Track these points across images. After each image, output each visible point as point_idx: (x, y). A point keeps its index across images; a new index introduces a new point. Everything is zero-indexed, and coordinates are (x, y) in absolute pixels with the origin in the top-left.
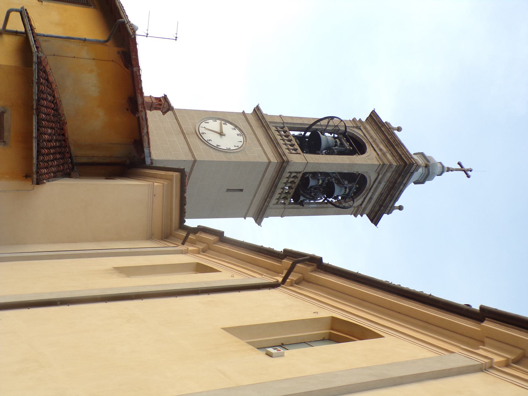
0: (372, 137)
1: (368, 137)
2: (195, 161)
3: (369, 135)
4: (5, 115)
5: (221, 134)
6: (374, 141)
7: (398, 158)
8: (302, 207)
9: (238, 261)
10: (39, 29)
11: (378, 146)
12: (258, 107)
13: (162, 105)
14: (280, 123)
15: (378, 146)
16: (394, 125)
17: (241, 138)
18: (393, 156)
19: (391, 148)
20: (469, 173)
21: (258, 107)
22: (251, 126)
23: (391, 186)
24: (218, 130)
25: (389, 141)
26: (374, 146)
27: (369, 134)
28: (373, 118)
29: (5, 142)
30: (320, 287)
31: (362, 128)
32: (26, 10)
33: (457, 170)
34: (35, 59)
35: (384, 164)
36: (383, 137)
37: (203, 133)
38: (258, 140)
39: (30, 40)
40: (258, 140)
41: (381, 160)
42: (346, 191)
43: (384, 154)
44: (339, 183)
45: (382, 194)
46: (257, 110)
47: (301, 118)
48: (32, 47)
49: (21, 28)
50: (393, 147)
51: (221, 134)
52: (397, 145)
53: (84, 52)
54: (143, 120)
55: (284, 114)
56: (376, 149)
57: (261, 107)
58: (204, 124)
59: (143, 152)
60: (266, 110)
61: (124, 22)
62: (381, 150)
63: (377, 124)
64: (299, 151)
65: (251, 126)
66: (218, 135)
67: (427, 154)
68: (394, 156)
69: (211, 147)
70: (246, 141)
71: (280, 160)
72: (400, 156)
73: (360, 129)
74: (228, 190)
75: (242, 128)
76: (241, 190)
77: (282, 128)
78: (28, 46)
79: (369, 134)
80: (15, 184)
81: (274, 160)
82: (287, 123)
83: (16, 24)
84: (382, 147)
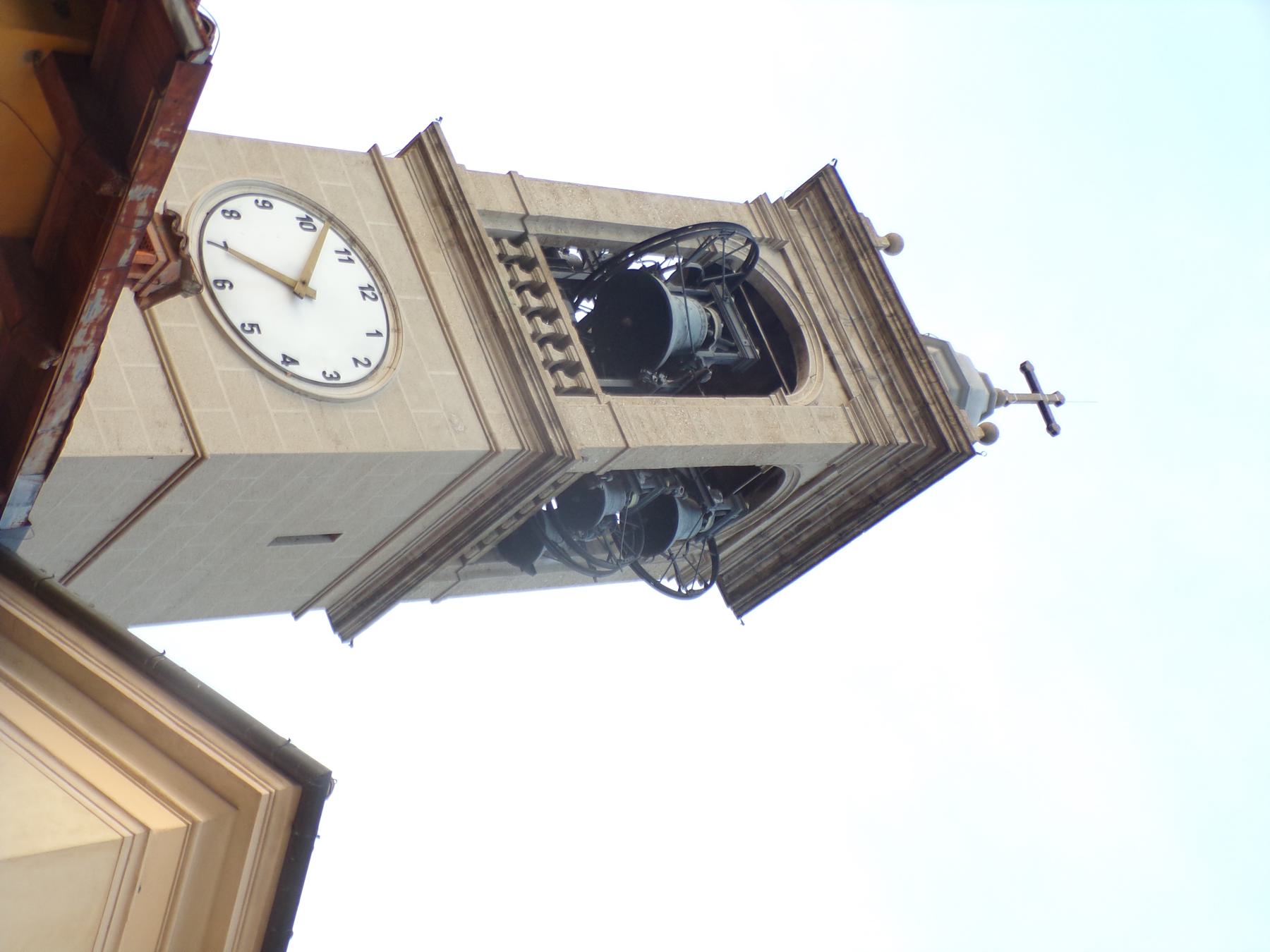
0: (823, 299)
1: (812, 298)
2: (196, 460)
3: (798, 274)
5: (298, 288)
6: (832, 321)
7: (913, 411)
8: (526, 576)
11: (845, 347)
12: (433, 129)
13: (152, 271)
14: (511, 216)
15: (845, 347)
17: (375, 314)
18: (896, 399)
20: (1052, 408)
21: (433, 129)
22: (410, 242)
23: (852, 504)
25: (884, 327)
26: (834, 347)
27: (814, 281)
28: (823, 195)
31: (788, 249)
33: (1022, 399)
35: (870, 444)
36: (862, 306)
37: (223, 283)
41: (863, 424)
42: (704, 525)
43: (867, 390)
44: (700, 506)
45: (808, 522)
46: (427, 149)
47: (585, 190)
51: (298, 288)
52: (914, 352)
54: (68, 378)
55: (527, 170)
56: (840, 359)
57: (449, 134)
58: (219, 228)
60: (470, 152)
62: (855, 366)
63: (842, 236)
64: (588, 376)
65: (410, 242)
66: (280, 292)
67: (958, 348)
68: (899, 401)
69: (262, 371)
70: (398, 330)
71: (533, 445)
72: (924, 406)
73: (783, 252)
74: (278, 540)
76: (332, 537)
77: (518, 240)
79: (814, 281)
81: (508, 442)
82: (537, 219)
84: (855, 343)
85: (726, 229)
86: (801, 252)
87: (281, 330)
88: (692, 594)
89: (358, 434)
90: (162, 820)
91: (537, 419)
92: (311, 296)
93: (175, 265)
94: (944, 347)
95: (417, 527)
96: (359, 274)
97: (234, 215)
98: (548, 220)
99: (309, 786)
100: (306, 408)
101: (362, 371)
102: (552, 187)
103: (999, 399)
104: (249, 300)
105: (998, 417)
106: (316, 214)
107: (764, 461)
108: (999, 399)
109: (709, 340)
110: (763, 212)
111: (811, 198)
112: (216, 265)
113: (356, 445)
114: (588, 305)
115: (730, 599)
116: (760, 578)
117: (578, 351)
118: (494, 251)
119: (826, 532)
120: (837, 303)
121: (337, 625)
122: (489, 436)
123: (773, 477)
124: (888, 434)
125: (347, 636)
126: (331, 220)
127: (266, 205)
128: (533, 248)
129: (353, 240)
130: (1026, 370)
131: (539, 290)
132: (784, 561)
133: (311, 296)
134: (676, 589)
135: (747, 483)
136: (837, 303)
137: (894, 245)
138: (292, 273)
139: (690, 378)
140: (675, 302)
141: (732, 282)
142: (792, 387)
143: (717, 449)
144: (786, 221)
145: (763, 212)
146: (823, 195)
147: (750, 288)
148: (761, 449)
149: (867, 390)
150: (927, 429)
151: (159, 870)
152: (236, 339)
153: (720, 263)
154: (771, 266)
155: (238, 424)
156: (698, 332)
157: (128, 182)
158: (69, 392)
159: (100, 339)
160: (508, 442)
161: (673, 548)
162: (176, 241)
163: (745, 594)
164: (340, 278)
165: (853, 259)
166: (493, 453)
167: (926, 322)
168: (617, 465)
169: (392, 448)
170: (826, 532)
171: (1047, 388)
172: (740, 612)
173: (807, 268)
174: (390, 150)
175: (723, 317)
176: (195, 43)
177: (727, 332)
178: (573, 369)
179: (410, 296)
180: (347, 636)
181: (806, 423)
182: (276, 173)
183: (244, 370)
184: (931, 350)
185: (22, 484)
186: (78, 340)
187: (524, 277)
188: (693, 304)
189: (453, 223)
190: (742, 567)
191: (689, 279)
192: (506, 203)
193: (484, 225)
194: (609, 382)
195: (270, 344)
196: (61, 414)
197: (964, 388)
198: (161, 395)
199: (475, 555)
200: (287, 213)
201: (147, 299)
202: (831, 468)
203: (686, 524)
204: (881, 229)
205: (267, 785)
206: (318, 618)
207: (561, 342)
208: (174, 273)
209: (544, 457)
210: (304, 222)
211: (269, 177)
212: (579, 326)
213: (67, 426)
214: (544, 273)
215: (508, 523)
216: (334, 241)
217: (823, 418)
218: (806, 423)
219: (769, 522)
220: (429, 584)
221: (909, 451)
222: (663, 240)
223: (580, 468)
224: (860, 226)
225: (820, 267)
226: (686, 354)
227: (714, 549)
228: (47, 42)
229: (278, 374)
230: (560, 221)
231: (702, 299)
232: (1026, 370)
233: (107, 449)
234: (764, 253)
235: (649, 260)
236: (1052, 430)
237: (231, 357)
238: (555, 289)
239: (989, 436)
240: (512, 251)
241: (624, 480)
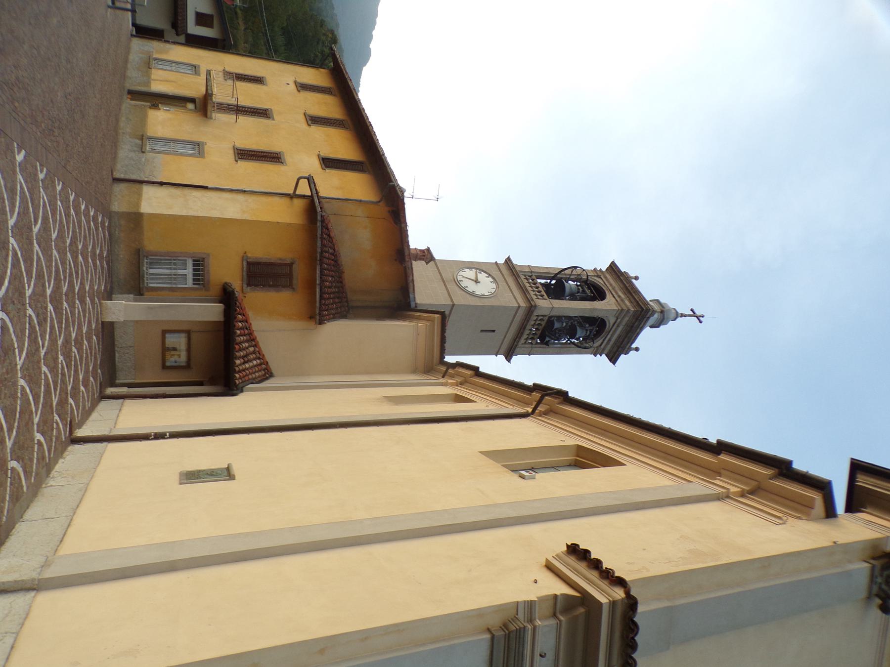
0: (611, 285)
2: (453, 305)
4: (294, 266)
5: (477, 281)
10: (323, 193)
11: (617, 293)
15: (617, 293)
17: (494, 285)
18: (631, 302)
27: (609, 282)
33: (690, 316)
34: (319, 218)
35: (622, 310)
44: (581, 326)
46: (508, 261)
51: (477, 281)
53: (360, 211)
58: (461, 273)
60: (516, 261)
62: (619, 296)
67: (662, 301)
74: (482, 331)
76: (494, 331)
79: (609, 282)
81: (523, 304)
84: (620, 294)
94: (658, 301)
120: (620, 294)
134: (330, 59)
165: (619, 277)
173: (607, 280)
184: (651, 303)
204: (632, 274)
221: (635, 312)
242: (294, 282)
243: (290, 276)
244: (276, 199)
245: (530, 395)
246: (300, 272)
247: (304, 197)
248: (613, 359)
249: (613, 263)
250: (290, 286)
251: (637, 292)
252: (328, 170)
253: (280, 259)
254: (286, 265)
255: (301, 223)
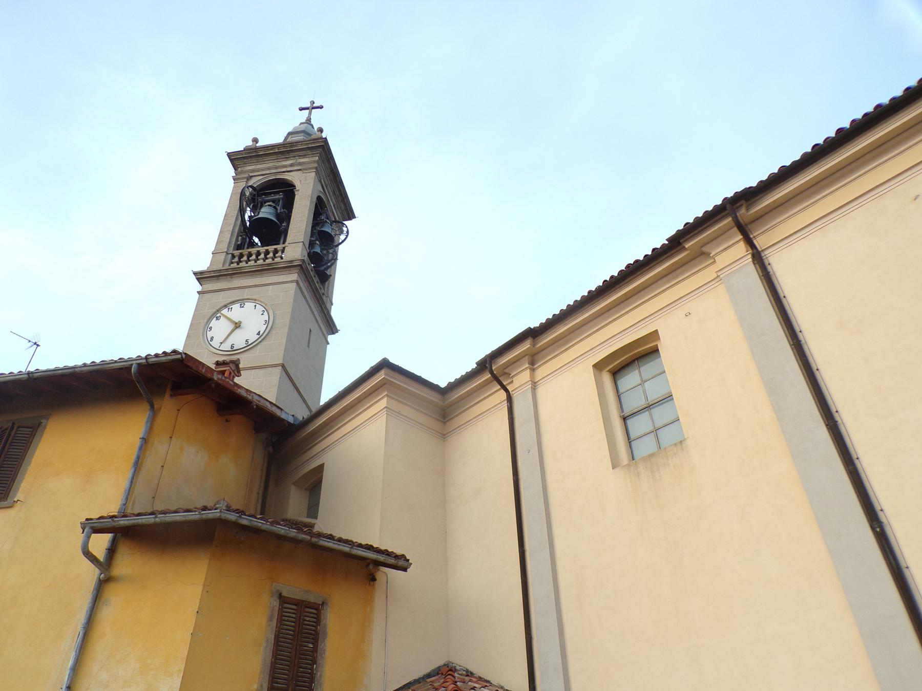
0: (269, 169)
2: (283, 366)
3: (261, 173)
4: (285, 594)
5: (237, 325)
6: (276, 168)
7: (309, 152)
9: (607, 315)
10: (112, 508)
12: (195, 274)
15: (285, 166)
16: (250, 143)
17: (249, 305)
19: (292, 154)
21: (195, 274)
24: (229, 327)
27: (263, 170)
28: (236, 159)
29: (323, 603)
30: (792, 201)
32: (87, 520)
33: (310, 114)
34: (232, 517)
35: (316, 168)
36: (273, 157)
37: (232, 347)
38: (256, 286)
39: (183, 519)
40: (256, 286)
41: (310, 168)
43: (300, 164)
46: (201, 277)
48: (204, 516)
49: (106, 538)
50: (292, 151)
51: (237, 325)
53: (160, 448)
56: (289, 169)
58: (215, 343)
59: (283, 420)
61: (139, 364)
62: (291, 165)
63: (250, 157)
64: (279, 247)
66: (237, 331)
67: (290, 129)
71: (297, 270)
75: (231, 300)
77: (233, 256)
78: (134, 534)
79: (263, 170)
80: (379, 601)
81: (294, 276)
83: (100, 543)
85: (242, 194)
86: (253, 171)
87: (249, 333)
88: (348, 232)
89: (284, 319)
90: (383, 403)
91: (289, 267)
92: (240, 322)
93: (231, 365)
94: (290, 134)
95: (310, 302)
96: (236, 307)
97: (212, 338)
98: (229, 246)
99: (385, 364)
100: (274, 332)
101: (266, 313)
102: (219, 242)
103: (309, 120)
104: (239, 340)
105: (316, 124)
106: (216, 314)
107: (315, 200)
108: (309, 120)
109: (275, 207)
110: (238, 179)
111: (236, 163)
112: (226, 346)
113: (287, 320)
114: (256, 240)
115: (350, 219)
116: (346, 209)
117: (271, 248)
118: (235, 265)
119: (338, 187)
120: (271, 165)
121: (333, 333)
122: (292, 282)
123: (319, 198)
124: (314, 162)
125: (337, 331)
126: (218, 311)
127: (211, 328)
128: (237, 253)
129: (225, 306)
130: (301, 109)
131: (250, 255)
132: (343, 201)
133: (240, 322)
135: (320, 208)
136: (271, 165)
137: (255, 140)
138: (232, 326)
139: (285, 216)
140: (261, 215)
141: (259, 195)
142: (294, 186)
143: (309, 215)
144: (242, 172)
145: (238, 179)
146: (236, 159)
147: (261, 190)
148: (311, 202)
149: (300, 164)
150: (313, 148)
151: (396, 406)
152: (249, 347)
153: (252, 197)
154: (256, 181)
155: (275, 352)
156: (272, 210)
157: (211, 379)
158: (263, 401)
159: (251, 392)
160: (294, 276)
161: (333, 234)
162: (224, 363)
163: (350, 215)
164: (236, 313)
166: (297, 282)
167: (279, 139)
168: (307, 246)
169: (290, 311)
170: (338, 187)
171: (308, 105)
172: (354, 217)
174: (199, 288)
175: (269, 201)
176: (179, 356)
177: (273, 201)
178: (276, 251)
179: (246, 294)
180: (337, 331)
181: (306, 187)
182: (200, 324)
183: (259, 347)
184: (289, 140)
185: (283, 416)
186: (250, 398)
187: (245, 258)
188: (263, 210)
189: (225, 275)
190: (342, 213)
191: (255, 209)
192: (222, 257)
193: (227, 267)
194: (282, 241)
195: (253, 337)
196: (268, 404)
197: (304, 132)
198: (262, 371)
199: (323, 291)
200: (214, 323)
201: (238, 371)
202: (320, 181)
203: (327, 229)
205: (381, 376)
206: (330, 338)
207: (267, 252)
208: (232, 366)
209: (301, 267)
210: (217, 319)
211: (202, 325)
212: (262, 246)
213: (271, 403)
214: (245, 252)
215: (316, 280)
216: (225, 312)
217: (306, 180)
218: (306, 187)
219: (331, 203)
220: (328, 305)
221: (320, 157)
222: (242, 211)
223: (306, 258)
224: (247, 150)
225: (259, 167)
226: (278, 216)
227: (335, 221)
228: (168, 390)
229: (262, 337)
230: (230, 242)
231: (261, 207)
232: (301, 109)
233: (275, 390)
234: (250, 183)
235: (247, 218)
236: (321, 107)
237: (254, 349)
238: (250, 250)
239: (321, 130)
240: (236, 259)
241: (312, 244)
242: (311, 599)
243: (301, 605)
244: (107, 614)
245: (684, 249)
246: (297, 584)
247: (112, 551)
248: (350, 215)
249: (230, 155)
250: (317, 609)
251: (273, 147)
252: (20, 496)
253: (270, 619)
254: (281, 610)
255: (206, 562)
